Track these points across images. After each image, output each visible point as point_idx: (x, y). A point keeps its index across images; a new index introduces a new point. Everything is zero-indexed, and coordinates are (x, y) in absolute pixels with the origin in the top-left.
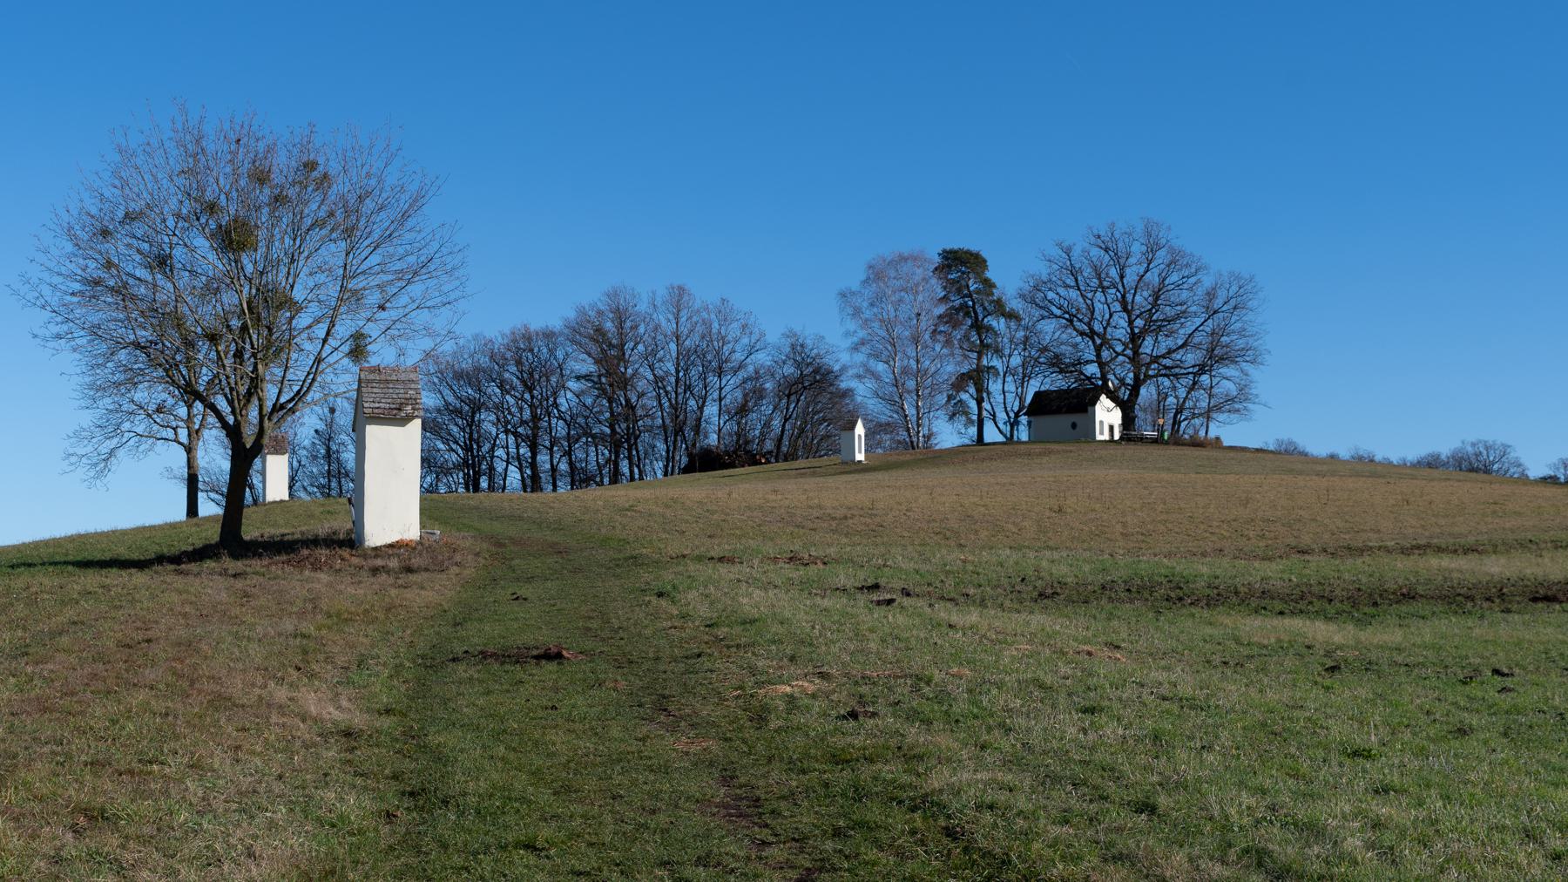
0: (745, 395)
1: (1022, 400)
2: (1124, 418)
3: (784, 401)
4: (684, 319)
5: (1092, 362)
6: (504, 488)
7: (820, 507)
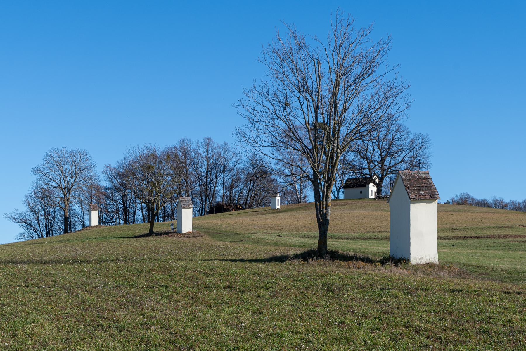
0: (233, 181)
1: (342, 181)
2: (378, 189)
3: (249, 183)
4: (210, 151)
5: (367, 168)
6: (134, 222)
7: (267, 224)
